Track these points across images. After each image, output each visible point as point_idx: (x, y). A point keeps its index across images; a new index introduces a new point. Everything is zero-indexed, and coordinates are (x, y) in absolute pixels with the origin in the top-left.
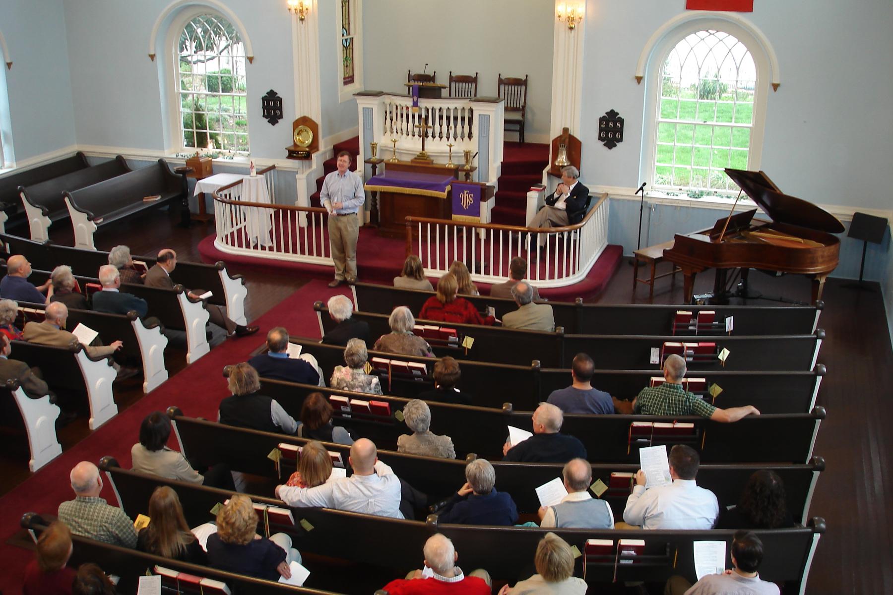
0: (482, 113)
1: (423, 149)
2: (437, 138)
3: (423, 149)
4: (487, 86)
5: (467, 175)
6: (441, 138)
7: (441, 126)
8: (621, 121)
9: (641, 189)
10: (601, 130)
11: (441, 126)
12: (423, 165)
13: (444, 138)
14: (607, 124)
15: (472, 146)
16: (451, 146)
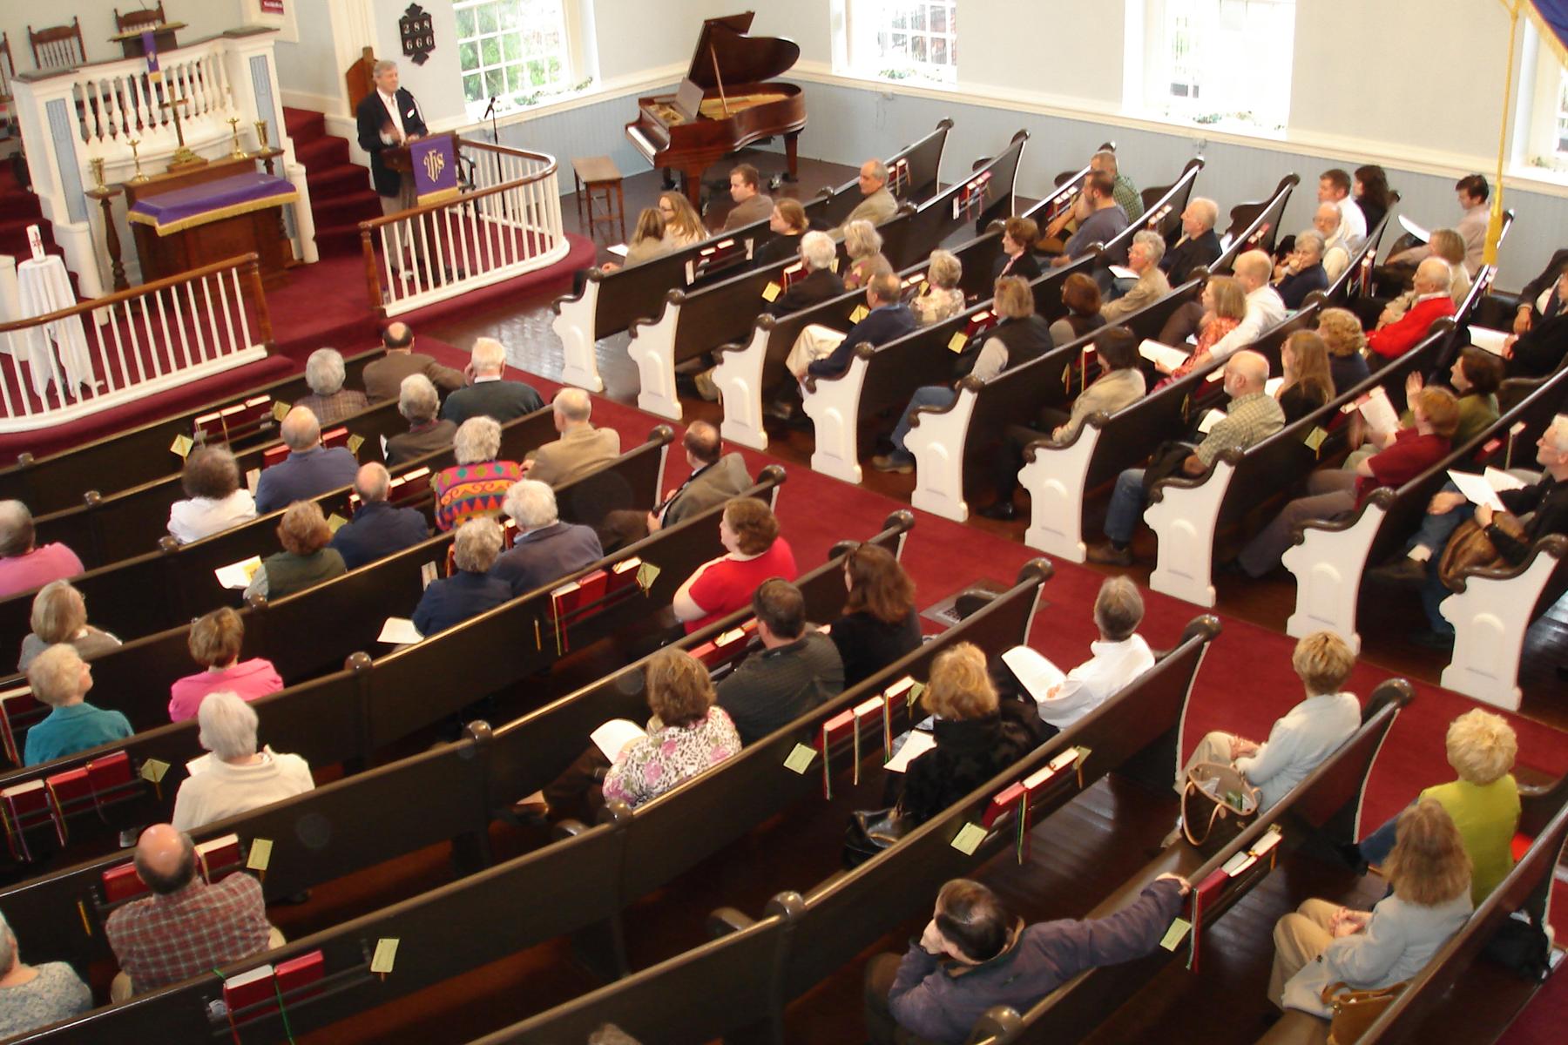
0: (50, 98)
1: (181, 143)
2: (107, 136)
3: (181, 143)
4: (99, 35)
5: (269, 164)
6: (114, 135)
7: (110, 114)
8: (428, 17)
9: (490, 108)
10: (404, 39)
11: (110, 114)
12: (187, 174)
13: (120, 134)
14: (412, 27)
15: (86, 154)
16: (133, 144)
